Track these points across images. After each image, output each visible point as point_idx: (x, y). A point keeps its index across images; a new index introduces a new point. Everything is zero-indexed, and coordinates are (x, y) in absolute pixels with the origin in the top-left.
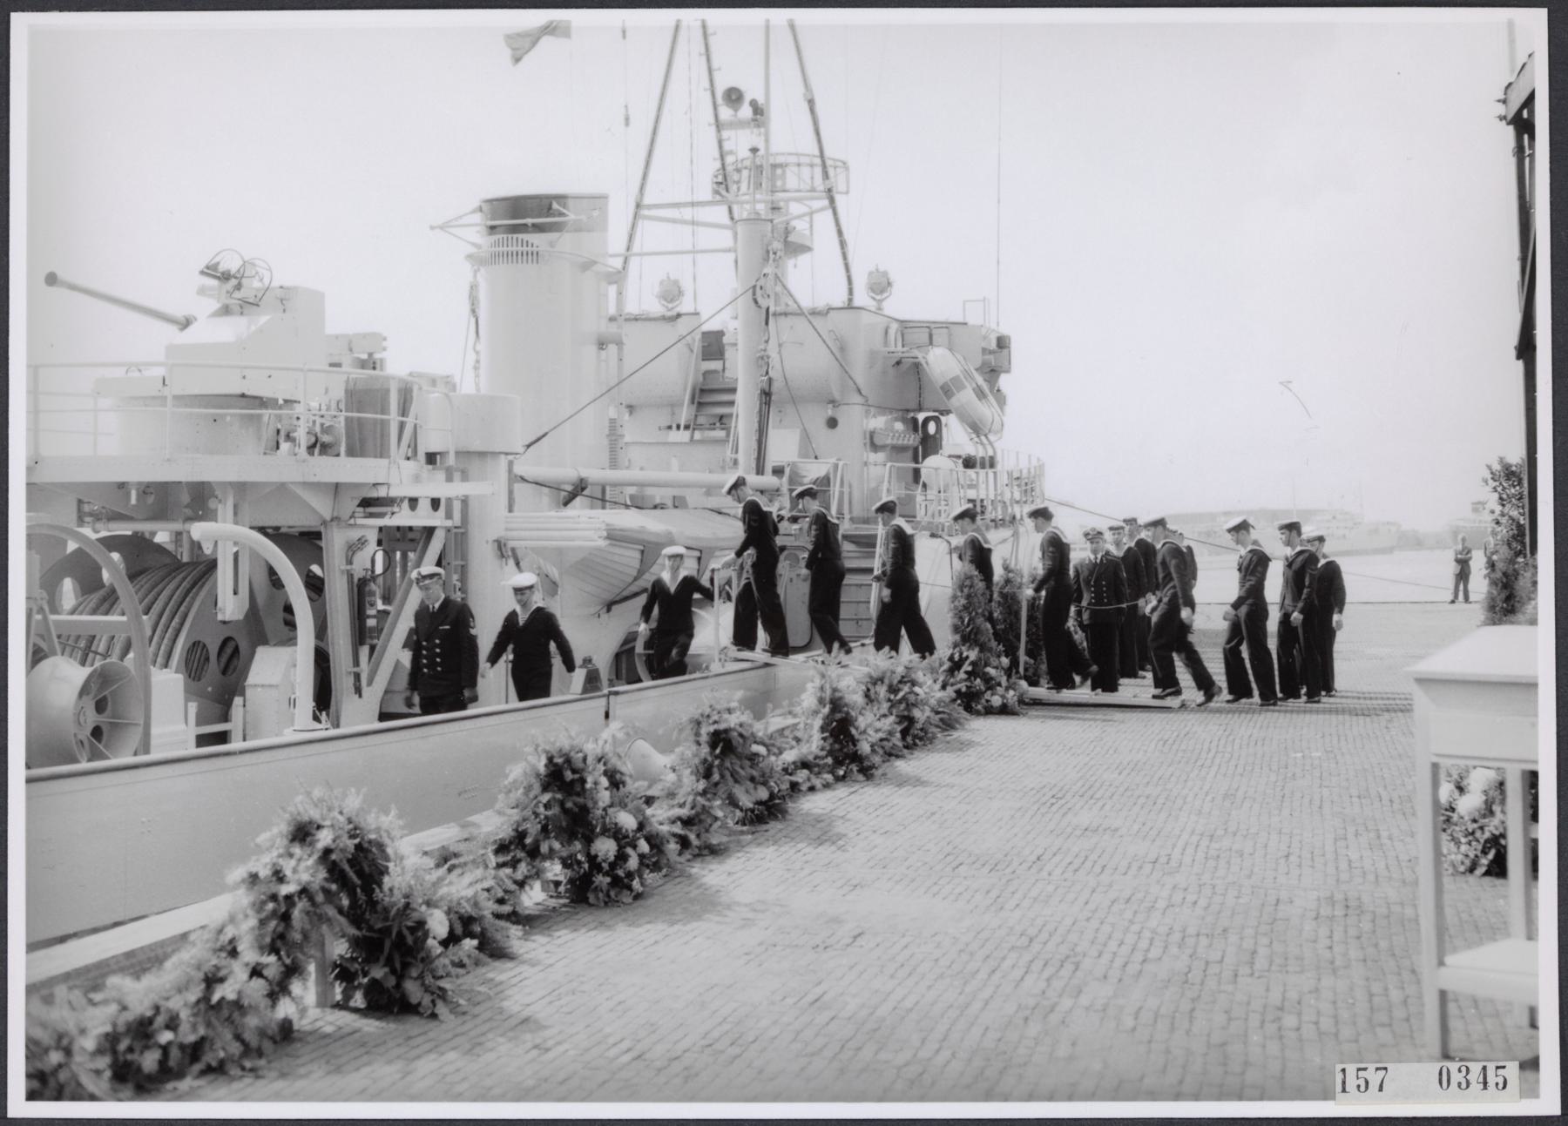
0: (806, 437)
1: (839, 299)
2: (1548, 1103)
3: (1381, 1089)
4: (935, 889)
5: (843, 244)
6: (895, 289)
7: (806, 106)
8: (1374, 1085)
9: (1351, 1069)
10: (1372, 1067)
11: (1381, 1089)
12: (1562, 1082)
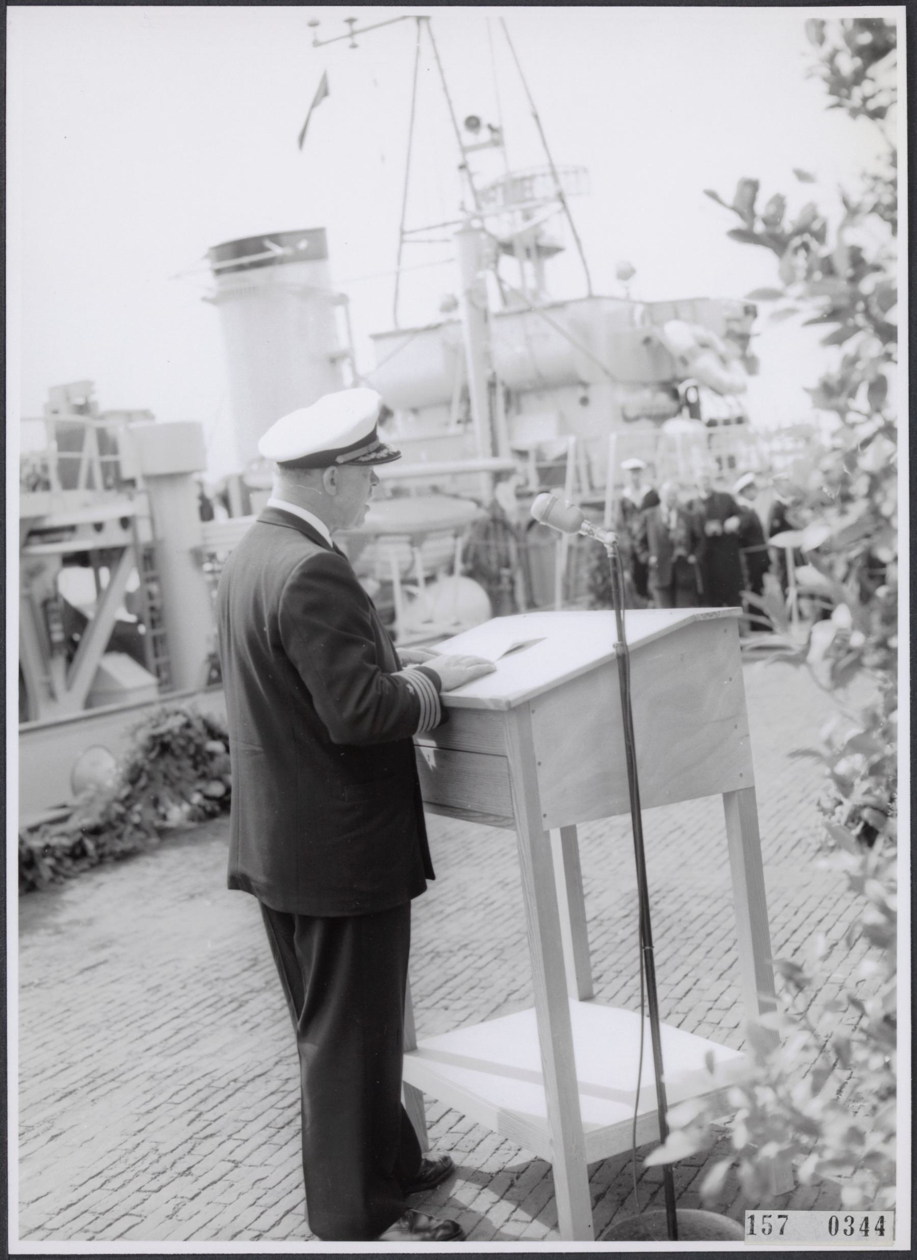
0: (562, 418)
1: (583, 293)
2: (902, 1242)
3: (782, 1232)
4: (59, 1026)
7: (532, 121)
11: (782, 1232)
12: (228, 1255)
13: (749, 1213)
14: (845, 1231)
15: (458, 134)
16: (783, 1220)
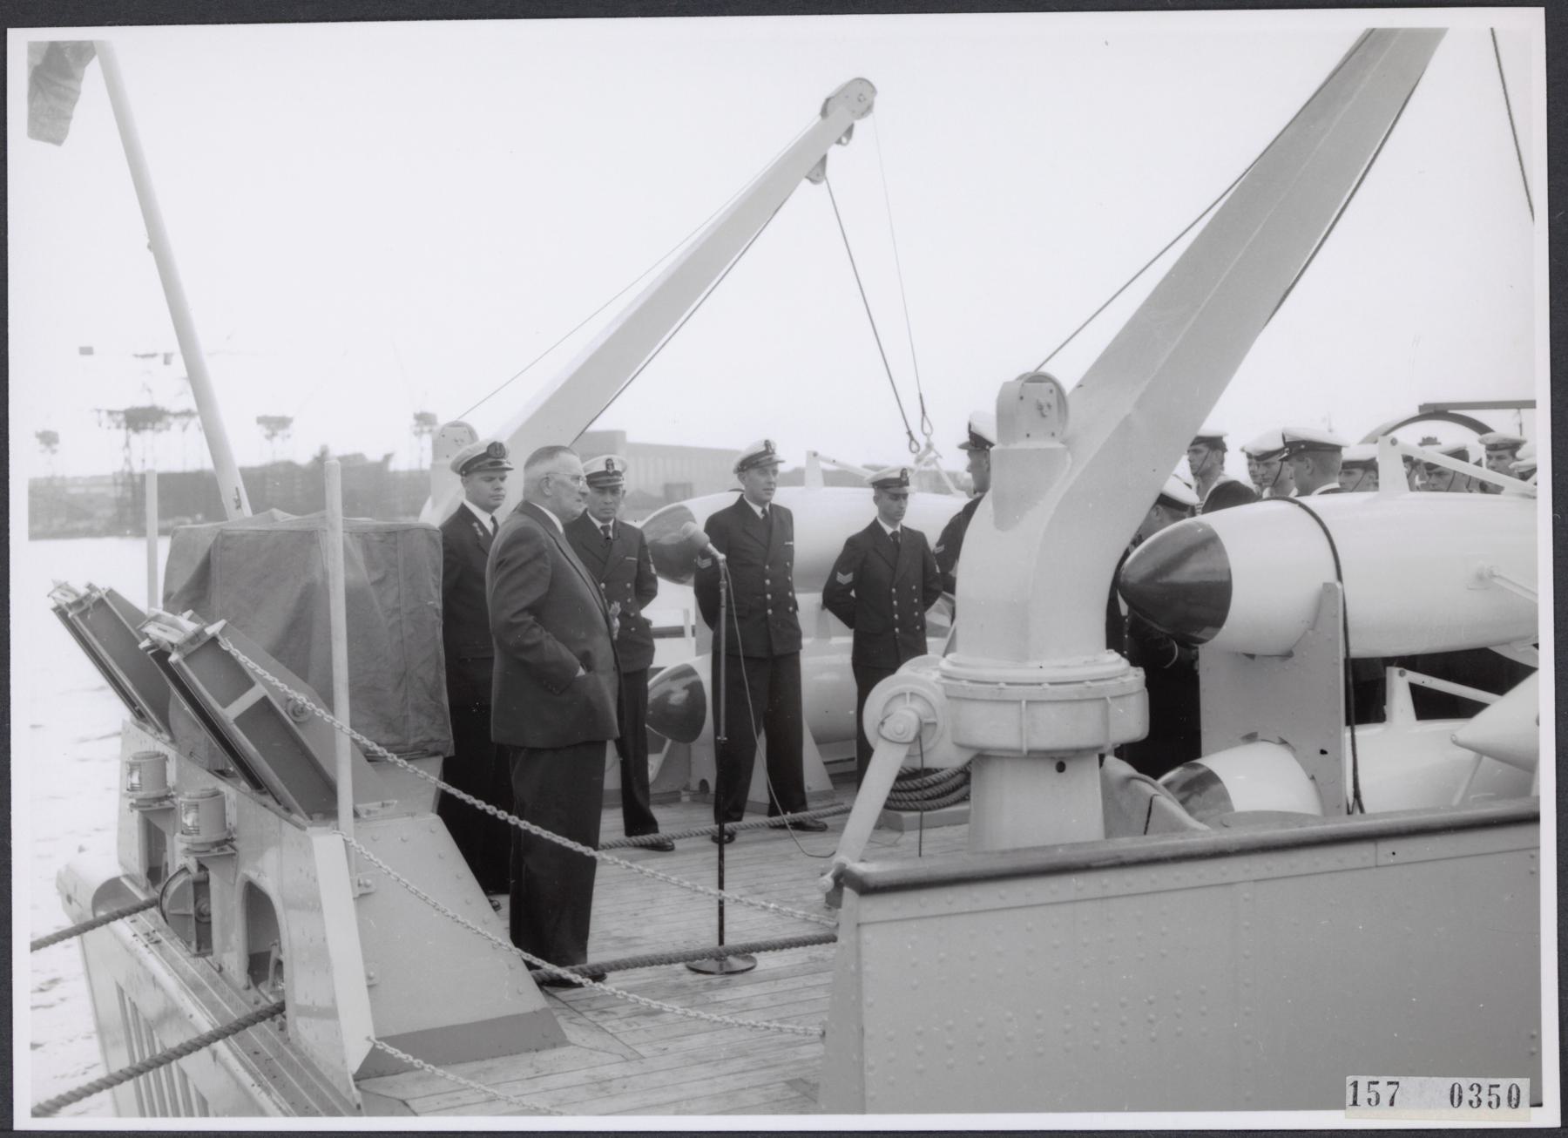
2: (1549, 1116)
3: (1392, 1104)
5: (157, 245)
9: (1363, 1081)
10: (1383, 1080)
11: (1392, 1104)
13: (1350, 1079)
14: (1471, 1103)
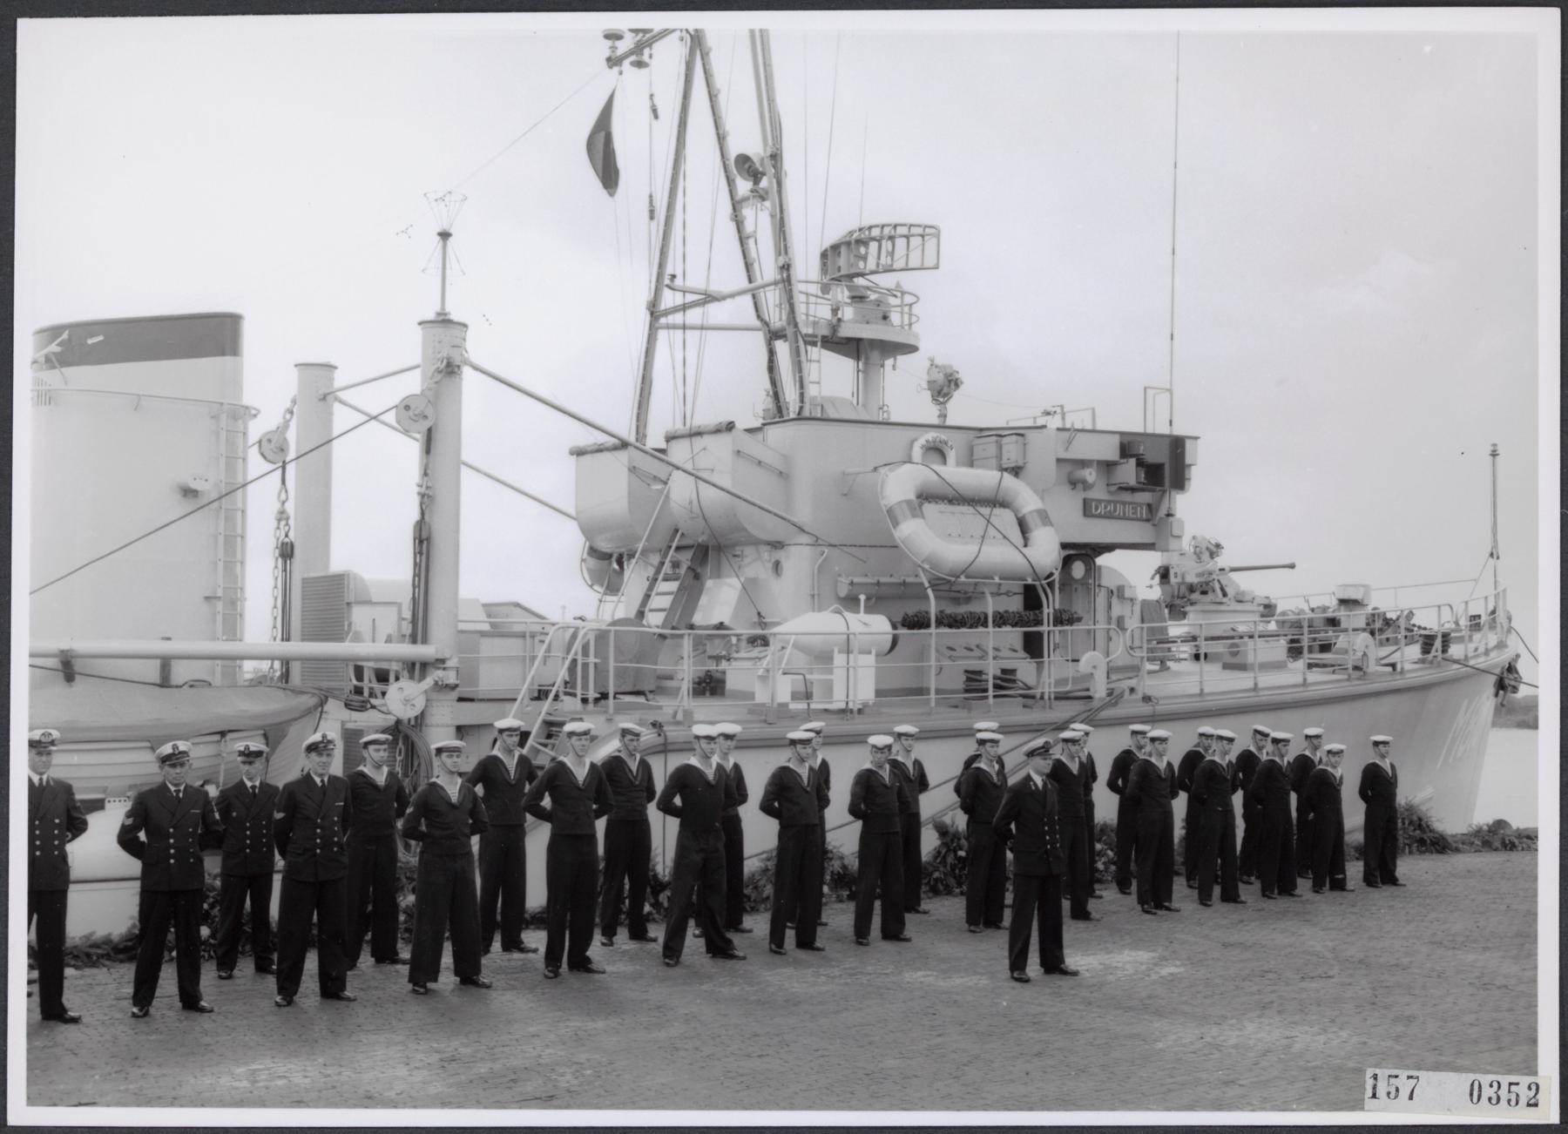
2: (1550, 1113)
3: (1411, 1098)
6: (962, 388)
8: (1405, 1093)
10: (1403, 1074)
11: (1411, 1098)
15: (730, 182)
16: (1413, 1082)
